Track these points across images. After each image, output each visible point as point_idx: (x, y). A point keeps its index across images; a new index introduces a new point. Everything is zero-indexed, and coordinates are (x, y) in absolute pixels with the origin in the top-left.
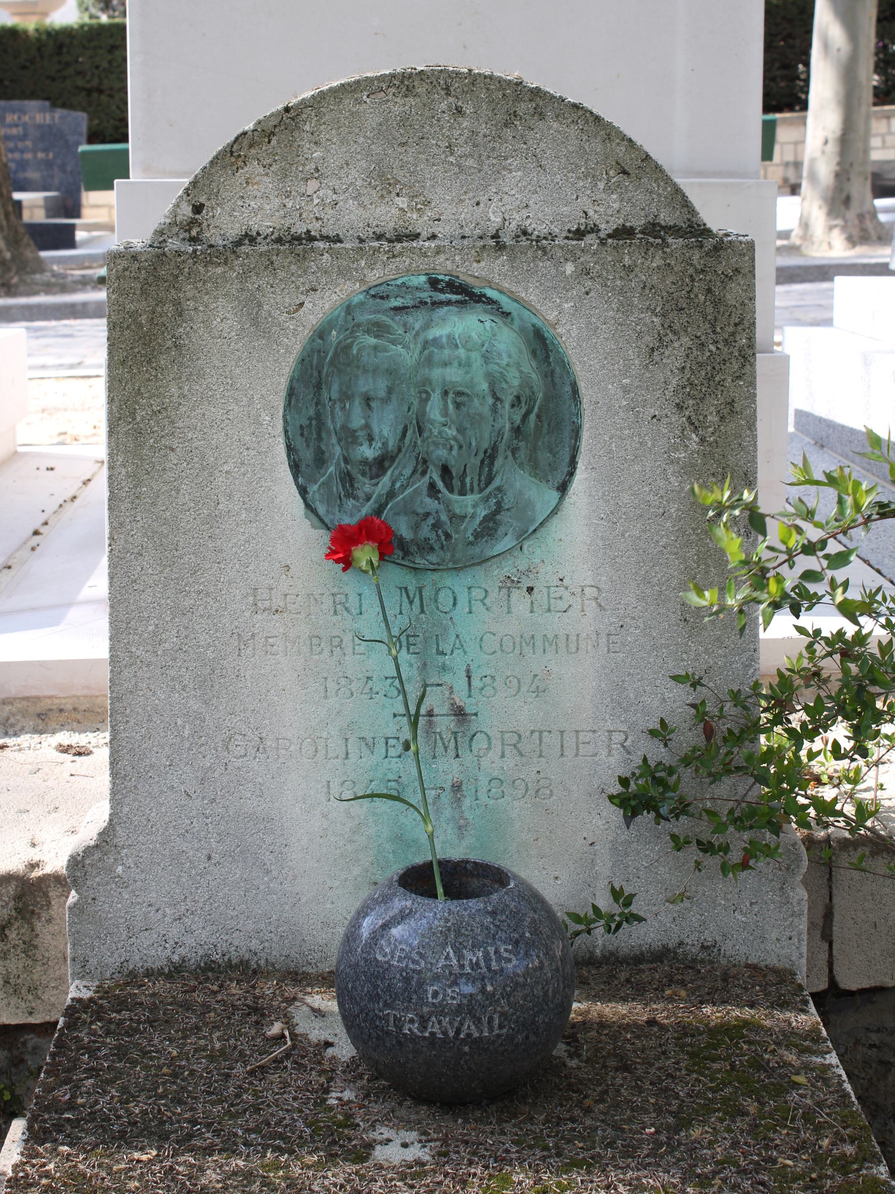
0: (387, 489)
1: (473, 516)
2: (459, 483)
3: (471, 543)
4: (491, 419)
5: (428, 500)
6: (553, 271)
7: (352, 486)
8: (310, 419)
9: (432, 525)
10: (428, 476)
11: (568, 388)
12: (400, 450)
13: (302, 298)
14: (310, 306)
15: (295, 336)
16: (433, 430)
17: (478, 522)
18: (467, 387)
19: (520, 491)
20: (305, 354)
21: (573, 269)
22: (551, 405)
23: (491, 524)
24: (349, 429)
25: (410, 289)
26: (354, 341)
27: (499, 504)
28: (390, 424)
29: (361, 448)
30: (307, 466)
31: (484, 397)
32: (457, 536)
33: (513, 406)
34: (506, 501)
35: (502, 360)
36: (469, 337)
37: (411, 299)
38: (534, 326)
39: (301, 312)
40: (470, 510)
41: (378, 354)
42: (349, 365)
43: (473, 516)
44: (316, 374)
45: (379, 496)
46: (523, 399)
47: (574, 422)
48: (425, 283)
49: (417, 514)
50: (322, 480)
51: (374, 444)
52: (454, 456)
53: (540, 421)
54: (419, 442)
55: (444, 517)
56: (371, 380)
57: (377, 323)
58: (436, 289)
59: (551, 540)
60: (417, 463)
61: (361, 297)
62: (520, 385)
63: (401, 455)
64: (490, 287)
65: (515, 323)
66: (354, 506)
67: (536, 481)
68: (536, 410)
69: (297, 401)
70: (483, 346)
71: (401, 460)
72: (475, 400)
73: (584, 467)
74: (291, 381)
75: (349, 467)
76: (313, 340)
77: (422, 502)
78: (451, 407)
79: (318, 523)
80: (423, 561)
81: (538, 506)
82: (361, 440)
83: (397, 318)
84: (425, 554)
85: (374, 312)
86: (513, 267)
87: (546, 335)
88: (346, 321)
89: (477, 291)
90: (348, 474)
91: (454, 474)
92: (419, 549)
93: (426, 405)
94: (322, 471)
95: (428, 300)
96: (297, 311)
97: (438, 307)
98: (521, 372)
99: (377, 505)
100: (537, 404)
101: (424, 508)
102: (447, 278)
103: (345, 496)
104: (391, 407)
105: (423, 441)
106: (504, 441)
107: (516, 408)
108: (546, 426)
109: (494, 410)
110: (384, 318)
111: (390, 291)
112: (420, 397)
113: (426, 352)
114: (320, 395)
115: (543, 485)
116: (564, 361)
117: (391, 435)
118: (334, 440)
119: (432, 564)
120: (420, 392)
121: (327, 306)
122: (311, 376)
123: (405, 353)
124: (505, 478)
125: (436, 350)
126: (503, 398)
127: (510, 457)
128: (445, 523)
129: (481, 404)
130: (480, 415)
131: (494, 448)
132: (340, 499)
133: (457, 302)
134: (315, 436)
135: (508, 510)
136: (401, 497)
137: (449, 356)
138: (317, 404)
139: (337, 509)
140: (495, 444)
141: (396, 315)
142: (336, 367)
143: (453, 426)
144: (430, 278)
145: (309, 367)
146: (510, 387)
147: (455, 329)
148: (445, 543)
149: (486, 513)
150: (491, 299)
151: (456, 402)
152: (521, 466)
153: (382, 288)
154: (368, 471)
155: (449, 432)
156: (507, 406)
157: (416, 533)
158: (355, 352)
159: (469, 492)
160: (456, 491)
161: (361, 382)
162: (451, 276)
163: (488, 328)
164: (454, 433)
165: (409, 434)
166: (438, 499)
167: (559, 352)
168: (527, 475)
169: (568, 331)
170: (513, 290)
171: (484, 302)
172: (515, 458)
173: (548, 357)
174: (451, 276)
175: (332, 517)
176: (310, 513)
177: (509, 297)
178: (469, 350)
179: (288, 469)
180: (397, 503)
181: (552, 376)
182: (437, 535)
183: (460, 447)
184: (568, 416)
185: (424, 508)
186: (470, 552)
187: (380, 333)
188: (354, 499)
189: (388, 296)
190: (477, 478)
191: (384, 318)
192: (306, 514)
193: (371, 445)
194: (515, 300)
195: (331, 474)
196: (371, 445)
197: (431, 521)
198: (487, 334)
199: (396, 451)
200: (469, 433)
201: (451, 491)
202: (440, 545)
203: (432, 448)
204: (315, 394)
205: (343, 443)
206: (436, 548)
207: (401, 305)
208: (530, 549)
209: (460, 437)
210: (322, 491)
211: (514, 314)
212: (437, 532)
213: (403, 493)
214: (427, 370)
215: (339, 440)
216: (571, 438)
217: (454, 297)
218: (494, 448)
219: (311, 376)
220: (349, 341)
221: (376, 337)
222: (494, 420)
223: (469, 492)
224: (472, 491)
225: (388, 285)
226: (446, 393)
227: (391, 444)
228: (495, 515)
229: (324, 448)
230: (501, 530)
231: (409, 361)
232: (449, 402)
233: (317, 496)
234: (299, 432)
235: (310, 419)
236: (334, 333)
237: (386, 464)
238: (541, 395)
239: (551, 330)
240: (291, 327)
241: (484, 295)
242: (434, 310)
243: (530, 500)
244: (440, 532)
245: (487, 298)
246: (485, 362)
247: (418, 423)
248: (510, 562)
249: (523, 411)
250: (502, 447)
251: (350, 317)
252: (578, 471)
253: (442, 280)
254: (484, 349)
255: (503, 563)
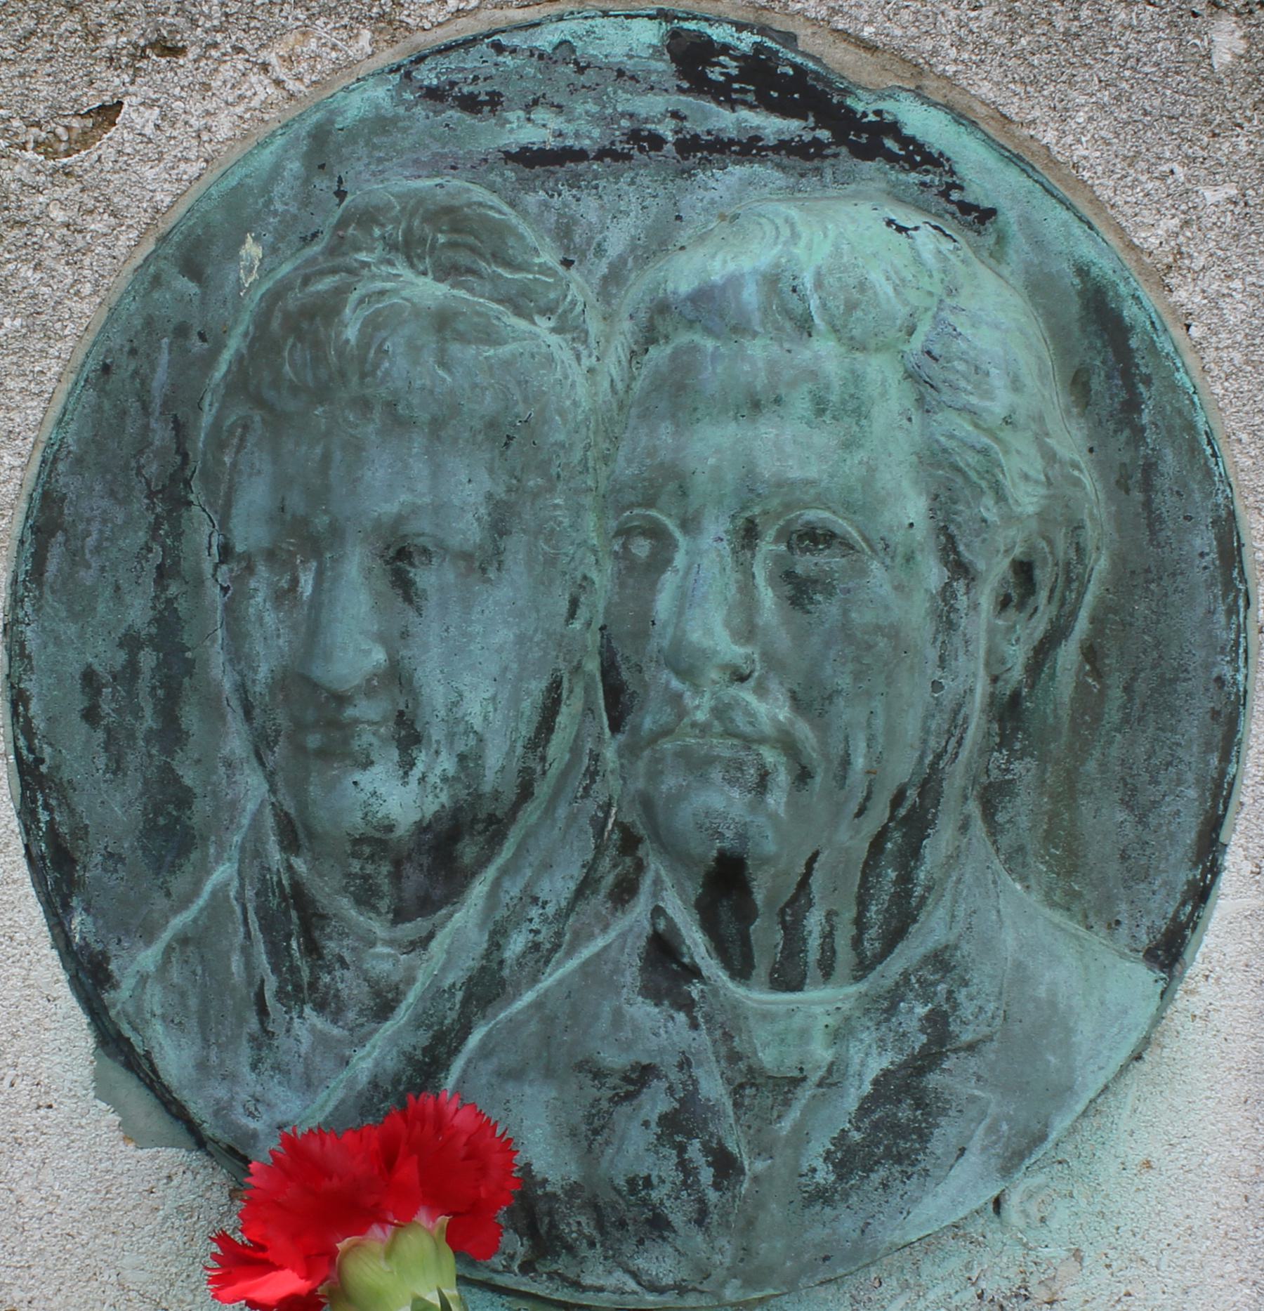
0: (469, 962)
1: (832, 1079)
2: (779, 936)
3: (822, 1196)
4: (933, 654)
5: (644, 1011)
6: (1165, 48)
7: (312, 949)
8: (131, 642)
9: (664, 1120)
10: (640, 909)
11: (1204, 541)
12: (526, 792)
13: (113, 82)
14: (144, 119)
15: (72, 257)
16: (689, 700)
17: (851, 1102)
18: (849, 507)
19: (1019, 966)
20: (118, 341)
21: (1241, 46)
22: (1141, 608)
23: (905, 1113)
24: (315, 686)
25: (590, 77)
26: (350, 288)
27: (938, 1024)
28: (494, 669)
29: (363, 777)
30: (112, 857)
31: (909, 558)
32: (760, 1166)
33: (1004, 603)
34: (967, 1010)
35: (988, 394)
36: (862, 286)
37: (596, 119)
38: (1082, 271)
39: (105, 147)
40: (821, 1053)
41: (455, 348)
42: (322, 394)
43: (832, 1079)
44: (161, 435)
45: (437, 993)
46: (1044, 576)
47: (1220, 680)
48: (656, 52)
49: (598, 1074)
50: (178, 922)
51: (422, 759)
52: (773, 817)
53: (1098, 674)
54: (610, 754)
55: (712, 1087)
56: (419, 468)
57: (449, 210)
58: (700, 85)
59: (1114, 1167)
60: (599, 850)
61: (380, 93)
62: (1041, 516)
63: (531, 813)
64: (918, 93)
65: (1012, 256)
66: (322, 1040)
67: (1073, 926)
68: (1082, 625)
69: (75, 557)
70: (911, 331)
71: (530, 834)
72: (875, 565)
73: (1248, 867)
74: (49, 464)
75: (300, 865)
76: (157, 281)
77: (618, 1015)
78: (767, 596)
79: (157, 1121)
80: (619, 1278)
81: (1085, 1030)
82: (365, 738)
83: (532, 200)
84: (628, 1248)
85: (435, 166)
86: (1012, 15)
87: (1130, 312)
88: (306, 200)
89: (861, 105)
90: (298, 896)
91: (759, 897)
92: (600, 1226)
93: (653, 587)
94: (179, 884)
95: (666, 130)
96: (84, 140)
97: (705, 163)
98: (1050, 457)
99: (424, 1038)
100: (1089, 598)
101: (628, 1046)
102: (746, 42)
103: (280, 994)
104: (504, 593)
105: (630, 752)
106: (964, 755)
107: (1011, 613)
108: (1116, 694)
109: (946, 619)
110: (479, 194)
111: (506, 80)
112: (625, 556)
113: (659, 354)
114: (178, 535)
115: (1097, 940)
116: (1191, 427)
117: (497, 719)
118: (236, 742)
119: (654, 1288)
120: (625, 532)
121: (224, 127)
122: (143, 443)
123: (566, 356)
124: (961, 912)
125: (709, 344)
126: (981, 565)
127: (978, 828)
128: (713, 1110)
129: (899, 588)
130: (894, 633)
131: (930, 785)
132: (263, 1011)
133: (784, 146)
134: (149, 721)
135: (971, 1047)
136: (529, 997)
137: (773, 367)
138: (163, 574)
139: (245, 1052)
140: (934, 765)
141: (526, 185)
142: (259, 402)
143: (773, 685)
144: (675, 34)
145: (133, 405)
146: (1010, 518)
147: (799, 251)
148: (712, 1196)
149: (885, 1064)
150: (920, 147)
151: (789, 576)
152: (1015, 859)
153: (471, 61)
154: (385, 885)
155: (761, 708)
156: (986, 600)
157: (589, 1155)
158: (351, 333)
159: (814, 972)
160: (762, 969)
161: (377, 473)
162: (763, 30)
163: (928, 256)
164: (784, 713)
165: (565, 718)
166: (687, 1005)
167: (1174, 388)
168: (1034, 899)
169: (1214, 302)
170: (1011, 111)
171: (891, 157)
172: (994, 829)
173: (1132, 405)
174: (763, 30)
175: (221, 1092)
176: (117, 1073)
177: (989, 141)
178: (856, 345)
179: (22, 872)
180: (514, 1025)
181: (1147, 486)
182: (684, 1165)
183: (803, 776)
184: (1200, 655)
185: (628, 1046)
186: (817, 1233)
187: (463, 258)
188: (320, 1007)
189: (495, 100)
190: (850, 913)
191: (479, 194)
192: (98, 1078)
193: (407, 764)
194: (1015, 159)
195: (219, 894)
196: (407, 764)
197: (656, 1102)
198: (925, 282)
199: (510, 794)
200: (846, 713)
201: (741, 970)
202: (691, 1208)
203: (671, 782)
204: (155, 527)
205: (278, 755)
206: (677, 1219)
207: (552, 143)
208: (1033, 1209)
209: (804, 731)
210: (175, 975)
211: (1009, 215)
212: (681, 1149)
213: (534, 980)
214: (665, 431)
215: (261, 746)
216: (1208, 747)
217: (772, 126)
218: (930, 785)
219: (143, 443)
220: (325, 284)
221: (446, 272)
222: (942, 662)
223: (814, 972)
224: (827, 968)
225: (499, 48)
226: (749, 534)
227: (494, 759)
228: (921, 1072)
229: (189, 777)
230: (945, 1134)
231: (582, 391)
232: (761, 580)
233: (154, 998)
234: (79, 702)
235: (131, 642)
236: (252, 250)
237: (468, 851)
238: (1101, 565)
239: (1149, 296)
240: (58, 215)
241: (893, 129)
242: (687, 173)
243: (1053, 1004)
244: (694, 1150)
245: (906, 141)
246: (920, 401)
247: (609, 669)
248: (955, 1264)
249: (1040, 626)
250: (956, 779)
251: (324, 184)
252: (1226, 883)
253: (725, 49)
254: (917, 342)
255: (926, 1268)
